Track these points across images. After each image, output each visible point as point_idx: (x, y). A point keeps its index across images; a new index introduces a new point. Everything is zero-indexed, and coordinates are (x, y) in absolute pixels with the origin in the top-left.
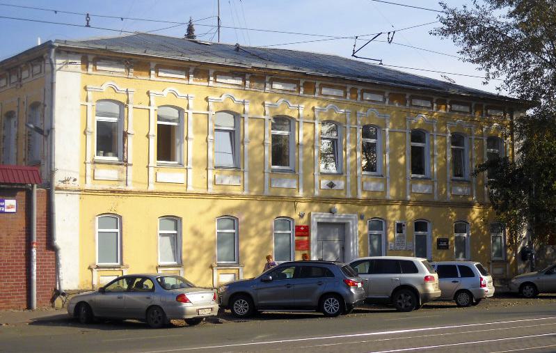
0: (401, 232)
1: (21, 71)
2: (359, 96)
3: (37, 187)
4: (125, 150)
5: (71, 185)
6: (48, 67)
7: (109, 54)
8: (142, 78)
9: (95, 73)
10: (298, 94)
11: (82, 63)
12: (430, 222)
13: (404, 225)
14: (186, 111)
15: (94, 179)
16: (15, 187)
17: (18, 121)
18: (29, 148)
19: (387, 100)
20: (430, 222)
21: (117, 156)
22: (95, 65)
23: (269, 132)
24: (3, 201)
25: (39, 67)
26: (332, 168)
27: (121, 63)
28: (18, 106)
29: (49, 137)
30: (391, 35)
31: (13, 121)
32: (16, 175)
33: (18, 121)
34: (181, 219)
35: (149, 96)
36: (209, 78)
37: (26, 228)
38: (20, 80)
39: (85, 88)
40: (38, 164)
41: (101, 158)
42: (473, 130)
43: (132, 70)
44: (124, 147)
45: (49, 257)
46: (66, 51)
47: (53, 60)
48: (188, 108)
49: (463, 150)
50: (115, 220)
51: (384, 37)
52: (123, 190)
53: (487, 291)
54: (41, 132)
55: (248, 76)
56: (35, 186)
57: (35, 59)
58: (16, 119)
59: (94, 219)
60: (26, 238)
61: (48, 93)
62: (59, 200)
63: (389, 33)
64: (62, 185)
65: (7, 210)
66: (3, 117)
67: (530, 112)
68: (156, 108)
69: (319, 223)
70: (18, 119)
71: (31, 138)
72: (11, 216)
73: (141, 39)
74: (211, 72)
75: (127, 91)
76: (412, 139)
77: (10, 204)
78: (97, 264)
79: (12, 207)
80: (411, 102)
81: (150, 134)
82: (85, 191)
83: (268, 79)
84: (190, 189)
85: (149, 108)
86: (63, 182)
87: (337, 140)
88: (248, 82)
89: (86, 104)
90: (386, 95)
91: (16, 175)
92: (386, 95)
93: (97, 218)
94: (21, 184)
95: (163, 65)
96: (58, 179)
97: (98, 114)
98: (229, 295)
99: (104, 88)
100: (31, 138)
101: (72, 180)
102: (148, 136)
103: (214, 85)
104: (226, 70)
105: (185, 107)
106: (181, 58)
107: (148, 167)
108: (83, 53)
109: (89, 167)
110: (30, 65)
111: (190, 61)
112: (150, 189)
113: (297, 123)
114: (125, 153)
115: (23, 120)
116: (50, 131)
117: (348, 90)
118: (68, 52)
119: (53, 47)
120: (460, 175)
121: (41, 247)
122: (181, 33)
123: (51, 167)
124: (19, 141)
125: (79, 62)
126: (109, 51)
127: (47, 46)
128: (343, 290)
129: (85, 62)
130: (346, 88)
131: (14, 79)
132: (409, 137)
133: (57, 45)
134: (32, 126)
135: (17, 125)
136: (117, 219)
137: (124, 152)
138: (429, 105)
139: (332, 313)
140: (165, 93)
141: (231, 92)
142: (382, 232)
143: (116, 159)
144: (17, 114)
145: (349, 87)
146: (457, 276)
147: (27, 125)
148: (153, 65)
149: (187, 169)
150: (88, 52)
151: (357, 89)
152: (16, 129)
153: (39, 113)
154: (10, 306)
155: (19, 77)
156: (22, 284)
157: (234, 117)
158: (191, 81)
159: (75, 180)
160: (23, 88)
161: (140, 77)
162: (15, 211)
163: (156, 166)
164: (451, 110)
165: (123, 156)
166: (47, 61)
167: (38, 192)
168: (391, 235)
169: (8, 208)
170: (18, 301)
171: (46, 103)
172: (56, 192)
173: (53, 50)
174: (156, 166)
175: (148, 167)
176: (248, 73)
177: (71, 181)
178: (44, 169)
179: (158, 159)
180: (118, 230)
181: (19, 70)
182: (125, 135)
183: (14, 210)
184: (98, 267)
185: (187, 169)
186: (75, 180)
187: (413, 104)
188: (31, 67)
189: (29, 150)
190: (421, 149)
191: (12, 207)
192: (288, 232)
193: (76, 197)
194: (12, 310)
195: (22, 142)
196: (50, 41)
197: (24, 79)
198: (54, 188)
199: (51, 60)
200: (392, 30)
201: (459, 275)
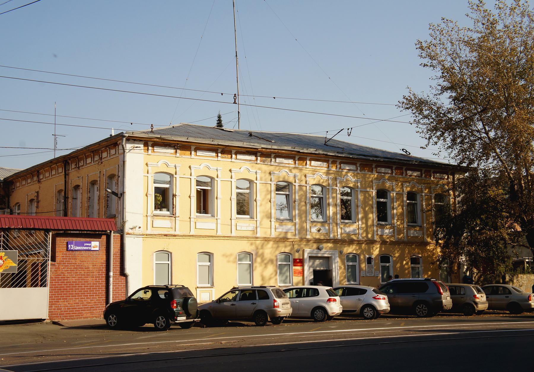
0: (371, 263)
1: (102, 153)
2: (404, 173)
3: (114, 233)
4: (174, 206)
5: (137, 231)
6: (121, 151)
7: (162, 141)
8: (186, 157)
9: (152, 154)
10: (305, 167)
11: (144, 146)
14: (216, 179)
15: (236, 230)
16: (98, 233)
17: (100, 187)
18: (107, 206)
19: (359, 168)
20: (391, 256)
21: (168, 210)
22: (196, 151)
24: (90, 242)
26: (320, 219)
27: (171, 147)
28: (100, 177)
29: (122, 198)
30: (349, 131)
31: (96, 187)
32: (59, 224)
33: (100, 187)
34: (213, 254)
35: (190, 169)
37: (106, 261)
38: (101, 159)
39: (147, 164)
40: (114, 217)
41: (158, 212)
42: (424, 189)
43: (178, 151)
44: (173, 204)
45: (96, 279)
46: (132, 139)
47: (124, 146)
48: (217, 177)
49: (416, 204)
50: (168, 255)
52: (173, 234)
53: (279, 312)
54: (116, 194)
55: (259, 154)
56: (113, 231)
57: (111, 145)
58: (98, 186)
60: (106, 268)
61: (121, 169)
62: (128, 241)
63: (348, 129)
64: (130, 231)
65: (92, 249)
66: (89, 184)
68: (196, 178)
70: (100, 185)
71: (108, 199)
72: (95, 253)
73: (186, 129)
74: (233, 152)
75: (256, 172)
76: (276, 189)
81: (191, 195)
82: (146, 235)
83: (273, 155)
84: (219, 233)
85: (231, 180)
86: (132, 229)
87: (322, 198)
88: (259, 158)
89: (147, 175)
90: (358, 165)
91: (59, 224)
92: (358, 165)
94: (103, 231)
95: (199, 147)
96: (127, 229)
97: (237, 188)
98: (263, 309)
99: (160, 164)
100: (108, 199)
101: (138, 227)
102: (190, 197)
103: (195, 158)
104: (243, 150)
105: (215, 177)
106: (212, 143)
107: (231, 219)
108: (145, 140)
110: (108, 148)
111: (218, 145)
112: (191, 234)
113: (255, 184)
114: (174, 209)
115: (103, 186)
116: (123, 194)
118: (135, 140)
119: (125, 136)
120: (416, 222)
121: (116, 274)
122: (214, 123)
123: (123, 219)
124: (100, 201)
125: (142, 146)
126: (163, 139)
127: (121, 136)
128: (374, 303)
129: (146, 145)
131: (97, 158)
133: (127, 135)
134: (109, 190)
135: (99, 190)
136: (169, 254)
137: (173, 208)
138: (390, 172)
139: (368, 317)
140: (202, 167)
141: (248, 165)
142: (357, 264)
143: (168, 213)
144: (99, 182)
146: (255, 299)
147: (106, 190)
148: (193, 148)
149: (217, 219)
150: (148, 140)
152: (98, 192)
153: (114, 182)
155: (101, 157)
156: (102, 300)
159: (140, 228)
160: (103, 164)
161: (184, 156)
162: (98, 250)
163: (195, 217)
164: (340, 168)
165: (173, 211)
166: (120, 147)
167: (114, 236)
168: (363, 266)
169: (94, 247)
170: (100, 312)
171: (120, 175)
172: (126, 236)
173: (125, 139)
174: (195, 217)
175: (231, 219)
176: (259, 152)
178: (119, 220)
180: (169, 262)
181: (100, 152)
182: (174, 196)
183: (97, 249)
185: (217, 219)
186: (140, 228)
189: (107, 207)
190: (385, 203)
192: (168, 262)
193: (140, 239)
194: (95, 318)
195: (103, 201)
196: (122, 133)
198: (125, 233)
199: (123, 145)
200: (350, 128)
201: (257, 298)
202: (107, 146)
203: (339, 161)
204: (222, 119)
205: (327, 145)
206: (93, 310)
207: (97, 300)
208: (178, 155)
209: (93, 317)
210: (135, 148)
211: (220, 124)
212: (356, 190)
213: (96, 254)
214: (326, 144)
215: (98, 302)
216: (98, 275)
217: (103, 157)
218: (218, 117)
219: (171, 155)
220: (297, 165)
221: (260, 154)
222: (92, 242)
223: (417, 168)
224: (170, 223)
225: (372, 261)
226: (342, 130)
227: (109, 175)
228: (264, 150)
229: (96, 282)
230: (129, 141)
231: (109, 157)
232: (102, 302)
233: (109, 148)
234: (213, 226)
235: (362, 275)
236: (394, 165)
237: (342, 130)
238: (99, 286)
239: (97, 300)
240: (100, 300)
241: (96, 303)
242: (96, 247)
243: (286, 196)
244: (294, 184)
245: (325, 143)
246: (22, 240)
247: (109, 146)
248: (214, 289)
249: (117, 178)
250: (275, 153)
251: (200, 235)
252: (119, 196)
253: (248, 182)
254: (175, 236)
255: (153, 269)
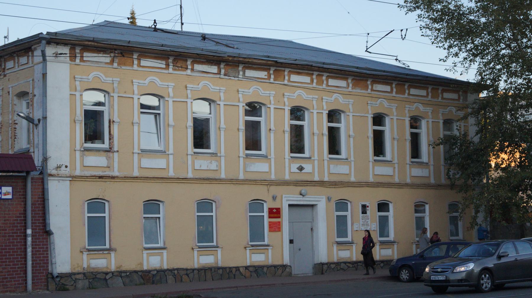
0: (366, 213)
5: (63, 171)
12: (391, 203)
13: (368, 207)
22: (139, 60)
23: (243, 118)
25: (26, 58)
30: (404, 33)
36: (239, 73)
41: (89, 145)
51: (397, 34)
59: (84, 203)
63: (402, 30)
64: (54, 172)
65: (3, 197)
67: (484, 94)
69: (290, 205)
71: (17, 126)
77: (7, 191)
78: (87, 247)
79: (8, 194)
80: (372, 87)
93: (86, 203)
100: (17, 126)
101: (64, 166)
102: (284, 131)
109: (78, 154)
117: (272, 72)
121: (35, 233)
130: (392, 84)
132: (370, 121)
145: (316, 73)
151: (438, 89)
154: (8, 289)
157: (210, 104)
158: (171, 70)
159: (66, 167)
160: (7, 78)
169: (5, 195)
172: (49, 178)
174: (193, 154)
177: (63, 168)
179: (247, 149)
183: (10, 197)
184: (89, 250)
187: (374, 88)
188: (16, 58)
191: (8, 194)
197: (8, 69)
200: (404, 28)
202: (14, 52)
203: (326, 74)
204: (136, 16)
205: (370, 53)
206: (7, 282)
207: (11, 268)
208: (115, 65)
209: (7, 291)
210: (58, 55)
211: (133, 18)
212: (348, 114)
213: (9, 204)
214: (368, 50)
215: (13, 271)
216: (13, 233)
217: (7, 68)
218: (131, 14)
219: (106, 66)
220: (287, 81)
221: (224, 64)
222: (3, 188)
223: (423, 85)
224: (107, 161)
225: (368, 210)
226: (392, 31)
227: (23, 90)
228: (230, 59)
229: (9, 243)
230: (50, 45)
231: (17, 67)
232: (18, 271)
233: (17, 54)
234: (213, 166)
235: (355, 229)
236: (394, 80)
237: (392, 31)
238: (14, 249)
239: (11, 268)
240: (15, 268)
241: (10, 271)
242: (8, 194)
243: (156, 117)
244: (218, 103)
245: (367, 49)
246: (327, 184)
247: (18, 51)
248: (166, 251)
249: (31, 97)
250: (244, 64)
251: (147, 176)
252: (35, 123)
253: (158, 99)
254: (113, 178)
255: (85, 225)
